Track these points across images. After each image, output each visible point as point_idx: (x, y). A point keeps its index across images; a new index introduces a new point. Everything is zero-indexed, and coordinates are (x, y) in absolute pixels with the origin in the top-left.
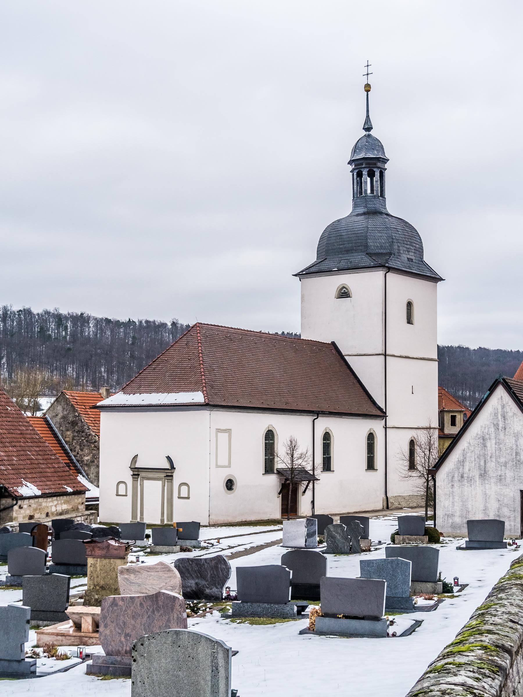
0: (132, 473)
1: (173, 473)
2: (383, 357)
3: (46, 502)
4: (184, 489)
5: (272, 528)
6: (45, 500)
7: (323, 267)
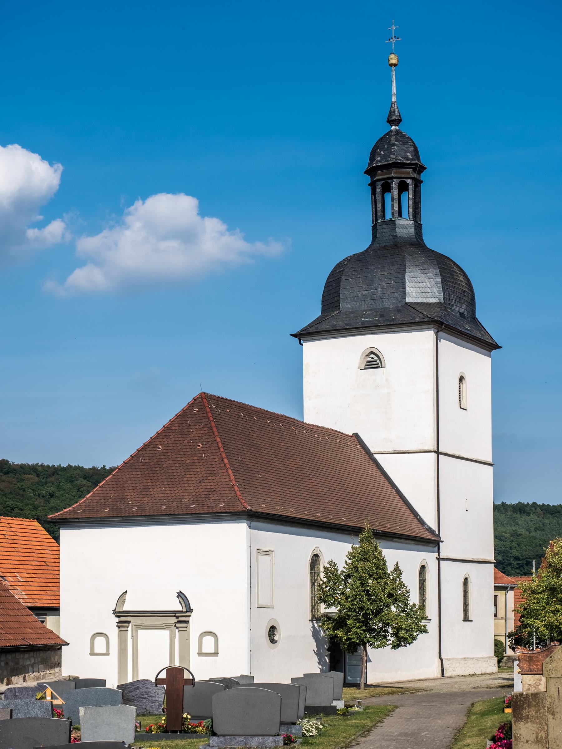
0: (117, 620)
1: (189, 616)
2: (440, 450)
3: (23, 658)
4: (208, 642)
5: (390, 685)
6: (22, 656)
7: (326, 326)
